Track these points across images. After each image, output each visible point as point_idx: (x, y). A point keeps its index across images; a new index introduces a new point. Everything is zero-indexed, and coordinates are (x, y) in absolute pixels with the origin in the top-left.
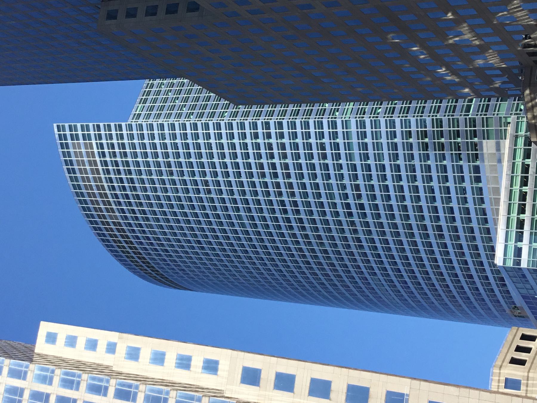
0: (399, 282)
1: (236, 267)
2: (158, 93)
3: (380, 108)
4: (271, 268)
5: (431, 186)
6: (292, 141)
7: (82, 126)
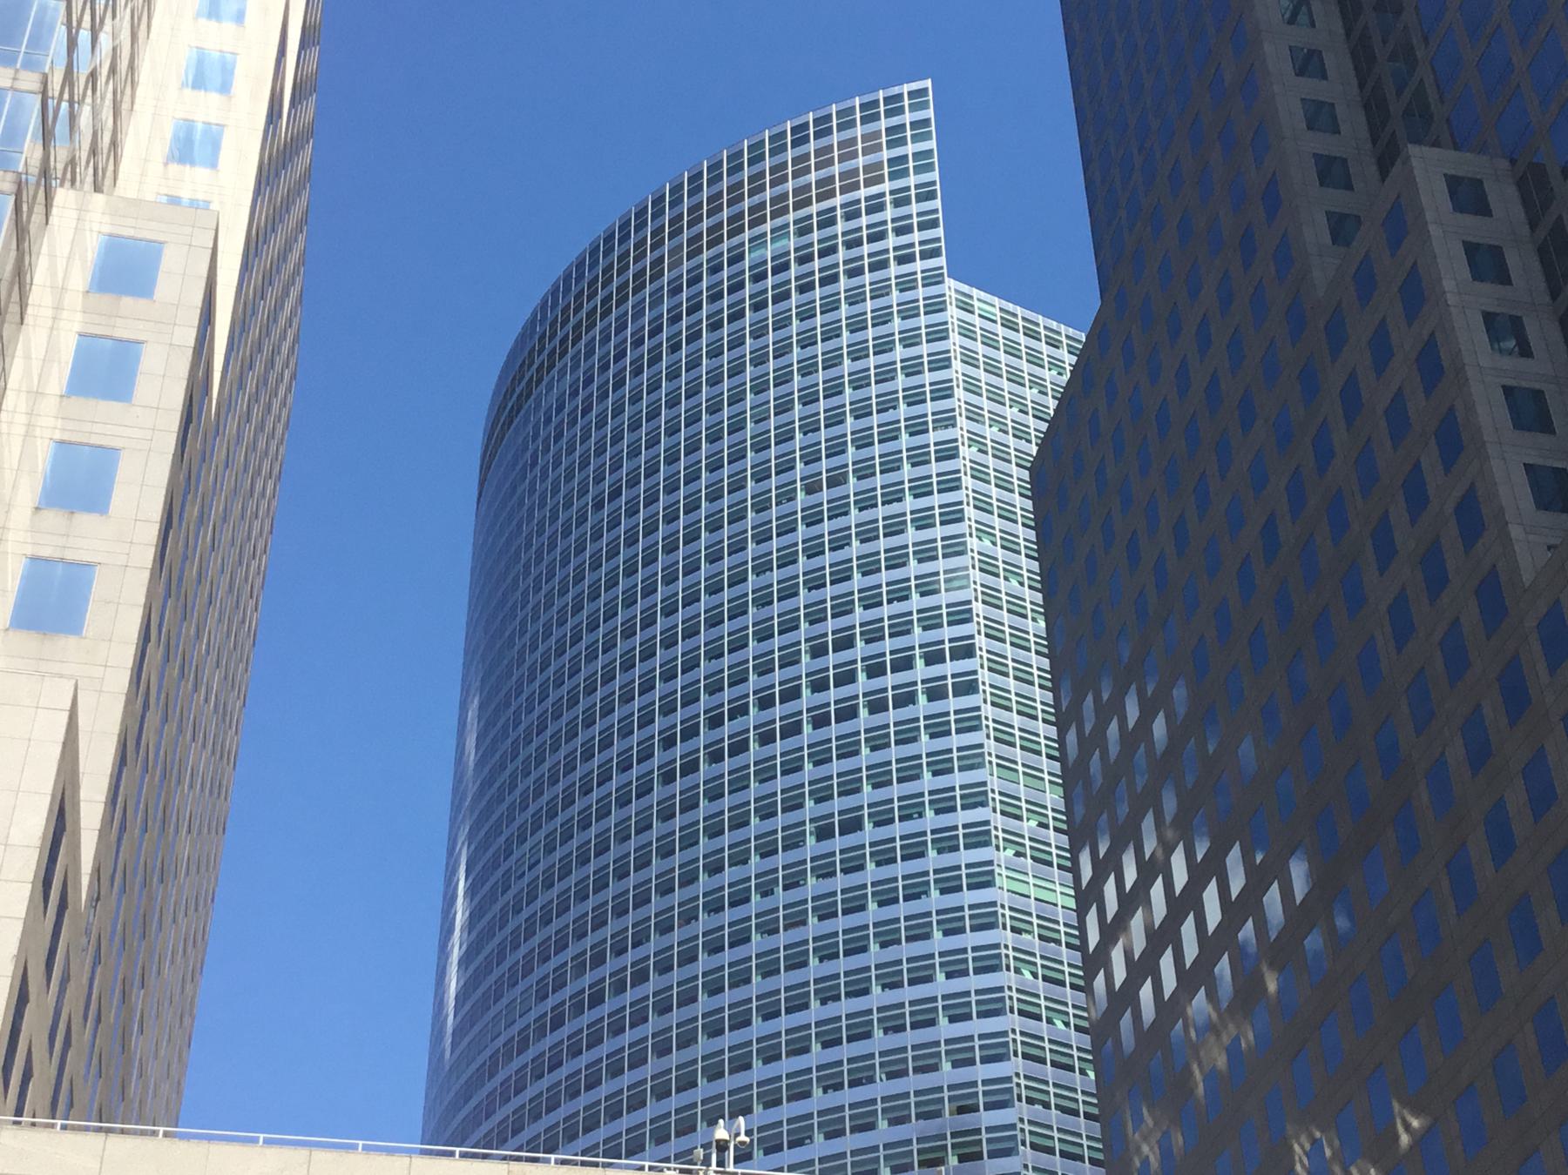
0: (523, 1030)
1: (540, 760)
2: (1035, 360)
3: (1035, 975)
4: (539, 903)
5: (810, 1138)
6: (929, 837)
7: (928, 153)
